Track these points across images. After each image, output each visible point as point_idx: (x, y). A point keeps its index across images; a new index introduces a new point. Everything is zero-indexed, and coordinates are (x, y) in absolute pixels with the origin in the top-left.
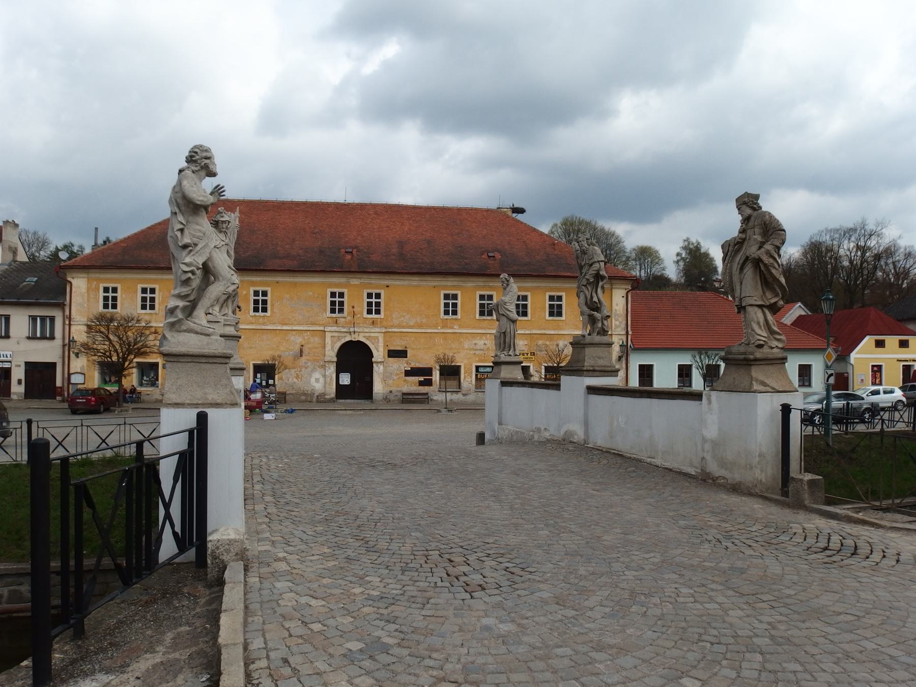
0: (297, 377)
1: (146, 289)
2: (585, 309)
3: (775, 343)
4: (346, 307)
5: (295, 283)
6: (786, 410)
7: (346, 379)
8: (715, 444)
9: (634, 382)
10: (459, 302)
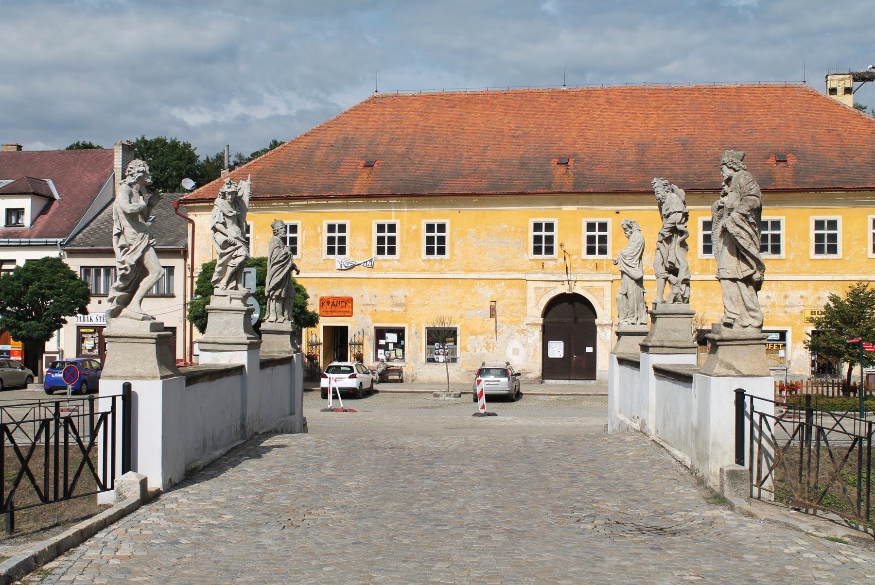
0: (487, 347)
4: (556, 245)
5: (485, 211)
6: (740, 394)
7: (557, 349)
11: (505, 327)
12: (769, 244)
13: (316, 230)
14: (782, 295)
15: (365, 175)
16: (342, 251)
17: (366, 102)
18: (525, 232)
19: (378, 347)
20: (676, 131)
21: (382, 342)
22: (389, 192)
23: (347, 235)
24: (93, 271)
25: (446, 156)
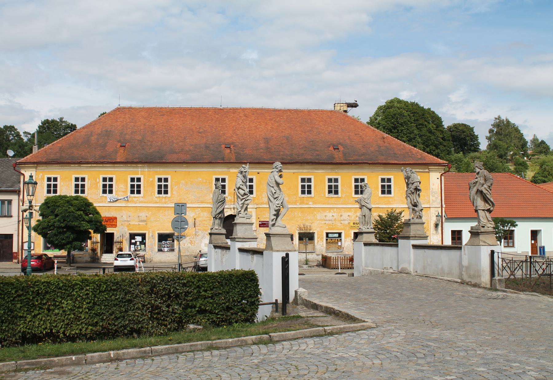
0: (191, 243)
1: (84, 181)
2: (411, 206)
3: (489, 225)
5: (189, 172)
6: (493, 252)
8: (467, 268)
9: (448, 241)
10: (312, 184)
11: (200, 232)
12: (333, 190)
13: (96, 180)
14: (340, 215)
15: (122, 151)
16: (111, 192)
17: (114, 111)
18: (211, 183)
19: (131, 243)
20: (282, 132)
21: (133, 241)
22: (137, 160)
23: (114, 183)
24: (6, 202)
25: (164, 141)
